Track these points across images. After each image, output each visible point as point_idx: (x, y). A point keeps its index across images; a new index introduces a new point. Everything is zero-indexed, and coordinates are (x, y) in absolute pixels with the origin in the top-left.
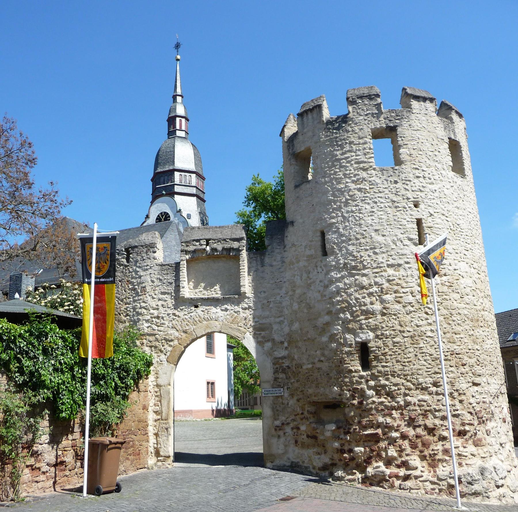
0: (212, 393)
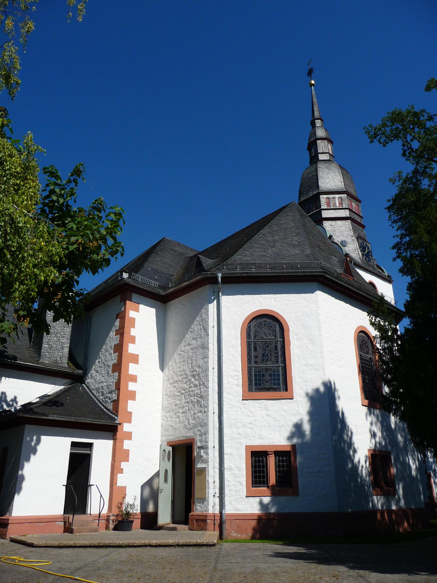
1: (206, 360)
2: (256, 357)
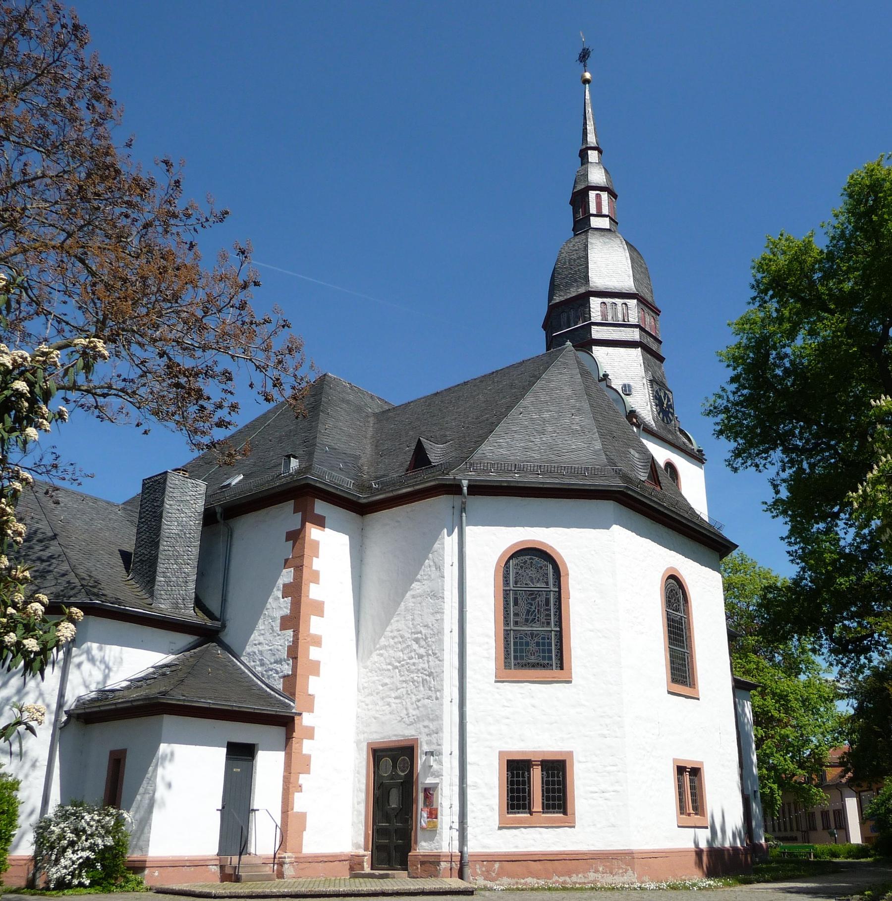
0: (694, 801)
1: (438, 616)
2: (516, 615)
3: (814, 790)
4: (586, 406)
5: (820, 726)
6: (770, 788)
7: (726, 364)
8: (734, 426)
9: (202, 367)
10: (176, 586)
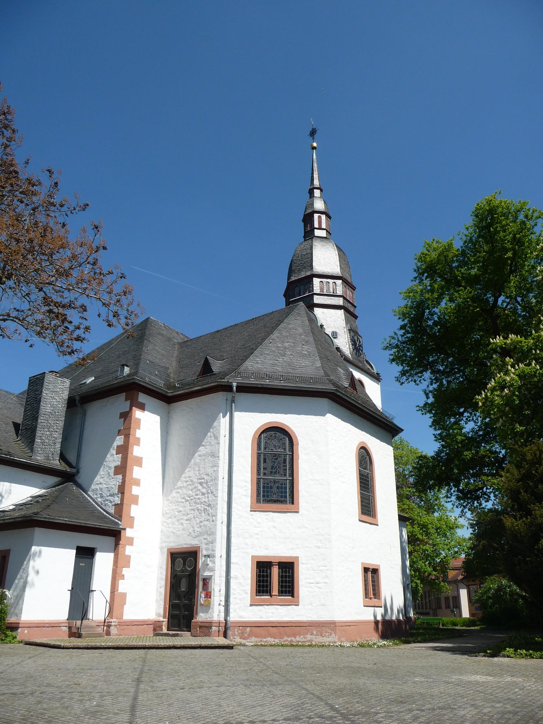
0: (374, 590)
1: (215, 468)
2: (265, 469)
3: (442, 584)
4: (311, 339)
5: (447, 545)
6: (416, 583)
7: (398, 317)
8: (401, 356)
9: (65, 301)
10: (48, 445)
